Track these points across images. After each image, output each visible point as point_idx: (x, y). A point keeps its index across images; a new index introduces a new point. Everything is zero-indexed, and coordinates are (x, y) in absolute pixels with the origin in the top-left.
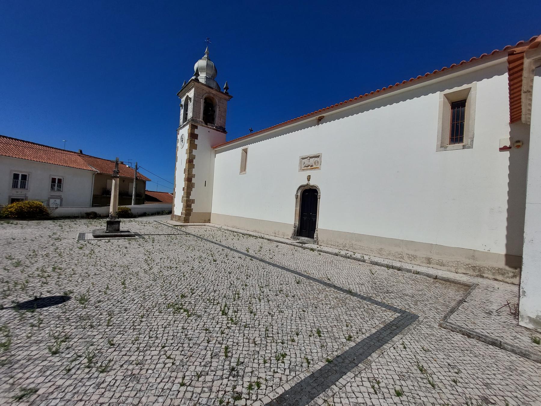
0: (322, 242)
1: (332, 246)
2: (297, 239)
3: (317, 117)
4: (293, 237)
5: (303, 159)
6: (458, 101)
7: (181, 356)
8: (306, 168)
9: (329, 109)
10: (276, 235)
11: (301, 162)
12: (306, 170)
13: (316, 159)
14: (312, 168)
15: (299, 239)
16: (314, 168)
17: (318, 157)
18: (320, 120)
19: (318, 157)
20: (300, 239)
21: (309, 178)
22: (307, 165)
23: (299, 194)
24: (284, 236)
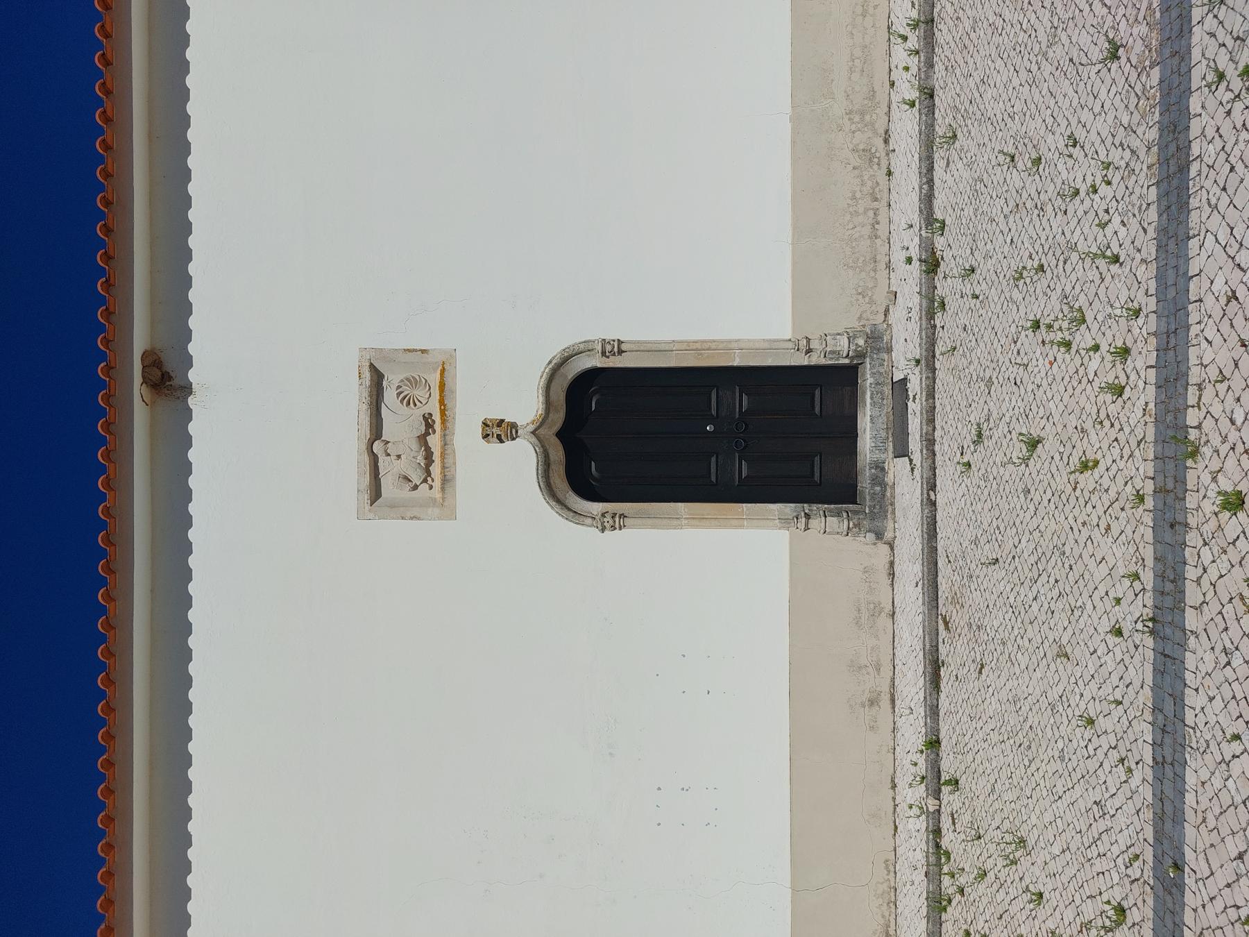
0: (872, 302)
1: (882, 231)
2: (879, 478)
3: (137, 386)
4: (873, 517)
5: (376, 492)
6: (541, 399)
7: (1211, 138)
8: (436, 469)
9: (118, 313)
10: (886, 688)
11: (400, 510)
12: (449, 461)
13: (390, 396)
14: (444, 422)
15: (879, 467)
16: (443, 413)
17: (377, 379)
18: (166, 377)
19: (377, 379)
20: (878, 456)
21: (497, 431)
22: (420, 459)
23: (596, 508)
24: (876, 611)
